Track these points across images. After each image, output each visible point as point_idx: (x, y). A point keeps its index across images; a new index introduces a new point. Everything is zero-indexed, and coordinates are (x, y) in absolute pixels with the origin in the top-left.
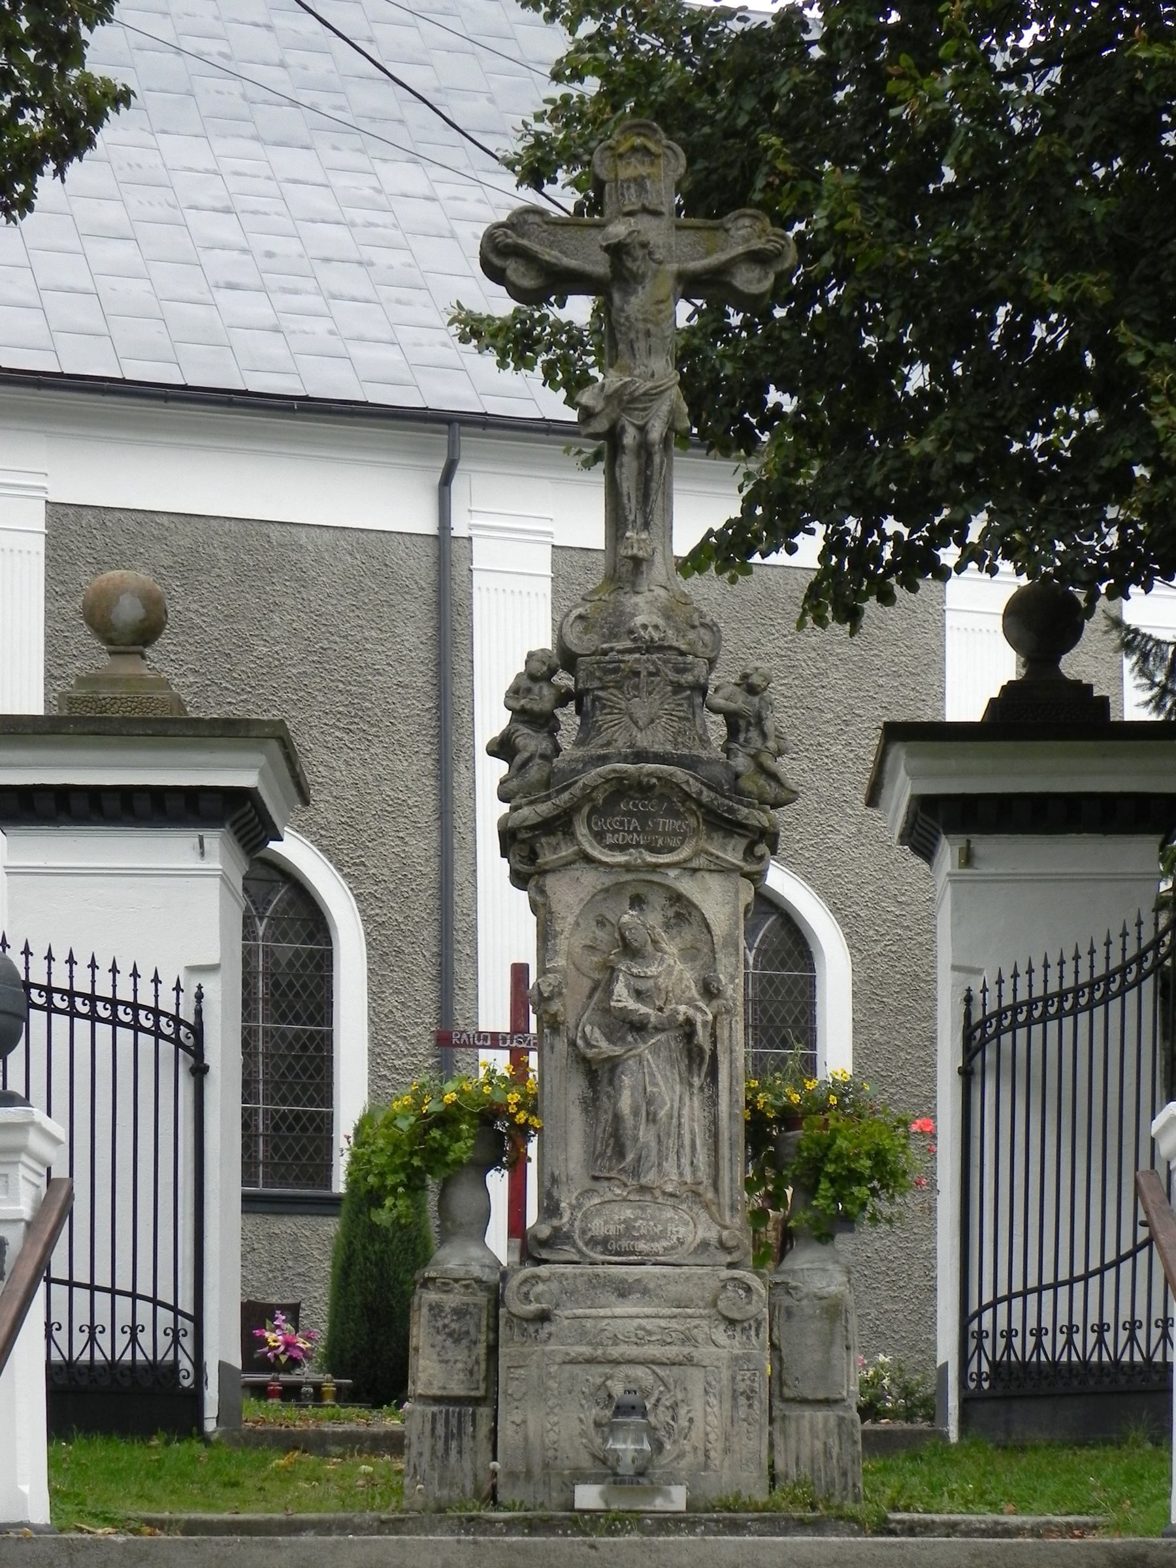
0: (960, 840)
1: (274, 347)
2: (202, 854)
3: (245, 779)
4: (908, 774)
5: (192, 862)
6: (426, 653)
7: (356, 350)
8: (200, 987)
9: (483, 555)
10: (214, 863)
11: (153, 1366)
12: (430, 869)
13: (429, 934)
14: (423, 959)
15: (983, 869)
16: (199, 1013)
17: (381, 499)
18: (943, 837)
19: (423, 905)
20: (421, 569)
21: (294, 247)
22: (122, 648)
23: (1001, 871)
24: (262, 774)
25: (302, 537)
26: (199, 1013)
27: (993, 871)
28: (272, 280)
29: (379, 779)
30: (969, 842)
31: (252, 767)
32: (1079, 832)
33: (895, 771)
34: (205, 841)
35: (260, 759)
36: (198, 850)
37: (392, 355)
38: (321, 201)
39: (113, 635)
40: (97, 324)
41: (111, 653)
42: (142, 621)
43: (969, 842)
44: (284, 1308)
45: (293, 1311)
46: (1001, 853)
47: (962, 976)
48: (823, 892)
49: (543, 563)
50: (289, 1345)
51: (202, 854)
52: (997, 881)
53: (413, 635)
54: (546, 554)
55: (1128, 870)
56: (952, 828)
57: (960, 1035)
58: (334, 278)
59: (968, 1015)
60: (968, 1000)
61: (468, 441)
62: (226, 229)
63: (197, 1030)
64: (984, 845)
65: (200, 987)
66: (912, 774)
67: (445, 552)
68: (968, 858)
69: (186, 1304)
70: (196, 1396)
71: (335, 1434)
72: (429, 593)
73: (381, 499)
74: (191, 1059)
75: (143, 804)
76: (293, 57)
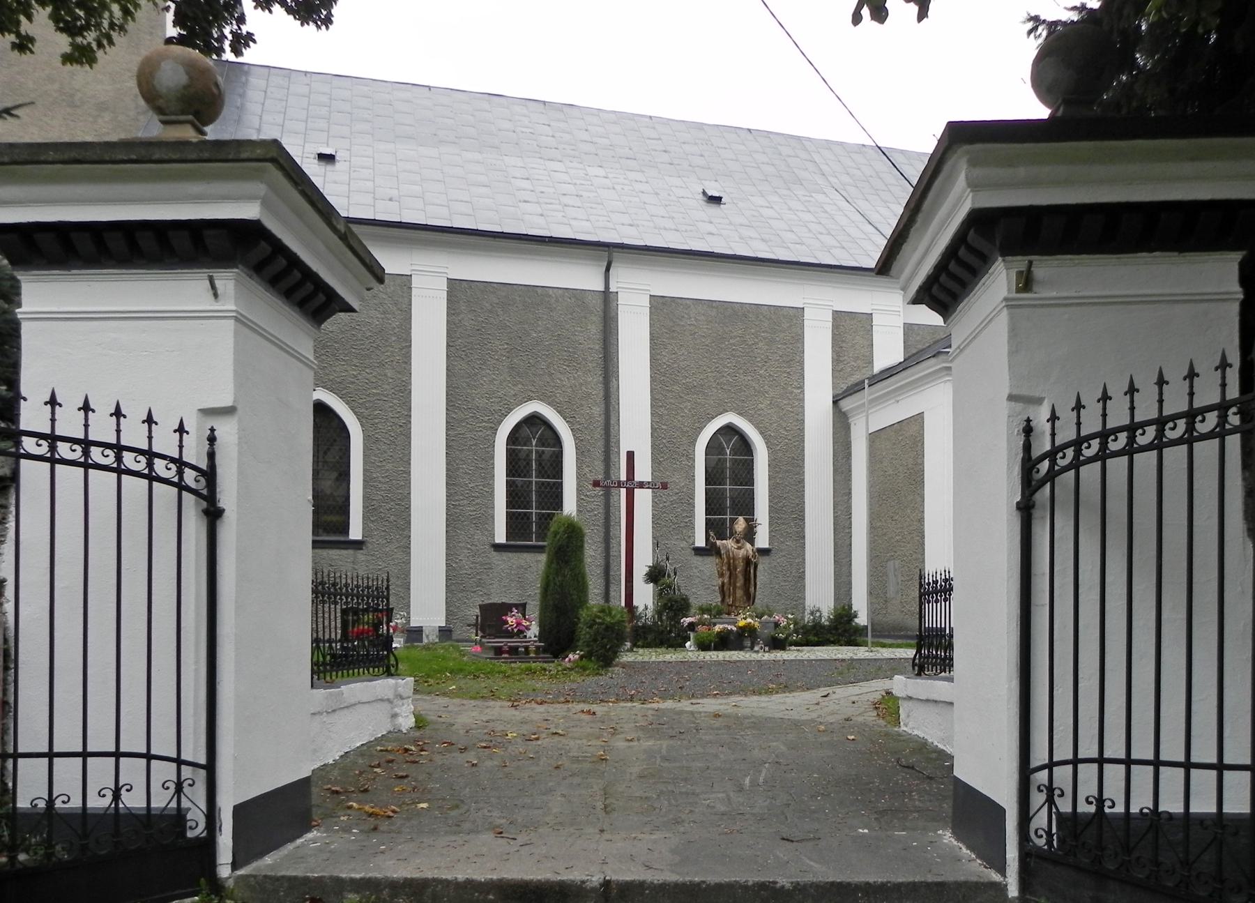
0: (1020, 262)
1: (541, 221)
2: (216, 295)
3: (248, 211)
4: (969, 185)
5: (207, 304)
6: (599, 336)
7: (573, 222)
8: (212, 430)
9: (622, 299)
10: (228, 305)
11: (148, 818)
12: (601, 419)
13: (601, 444)
14: (598, 453)
15: (1042, 292)
16: (211, 456)
17: (582, 277)
18: (1000, 259)
19: (599, 433)
20: (597, 304)
21: (552, 190)
22: (173, 118)
23: (1065, 294)
24: (265, 204)
25: (551, 292)
26: (211, 456)
27: (1054, 294)
28: (541, 200)
29: (581, 384)
30: (1031, 263)
31: (250, 198)
32: (1151, 250)
33: (951, 179)
34: (218, 283)
35: (260, 188)
36: (211, 292)
37: (588, 224)
38: (565, 177)
39: (161, 102)
40: (471, 212)
41: (164, 122)
42: (185, 87)
43: (1031, 263)
44: (516, 606)
45: (522, 607)
46: (1062, 275)
47: (1019, 406)
48: (757, 427)
49: (646, 302)
50: (519, 624)
51: (216, 295)
52: (1042, 306)
53: (594, 329)
54: (647, 299)
55: (1209, 290)
56: (1009, 249)
57: (1017, 469)
58: (565, 200)
59: (1027, 447)
60: (1028, 430)
61: (616, 255)
62: (526, 184)
63: (210, 475)
64: (1045, 268)
65: (212, 430)
66: (974, 185)
67: (607, 298)
68: (1026, 282)
69: (194, 750)
70: (208, 845)
71: (352, 880)
72: (601, 313)
73: (582, 277)
74: (204, 504)
75: (147, 242)
76: (557, 135)
